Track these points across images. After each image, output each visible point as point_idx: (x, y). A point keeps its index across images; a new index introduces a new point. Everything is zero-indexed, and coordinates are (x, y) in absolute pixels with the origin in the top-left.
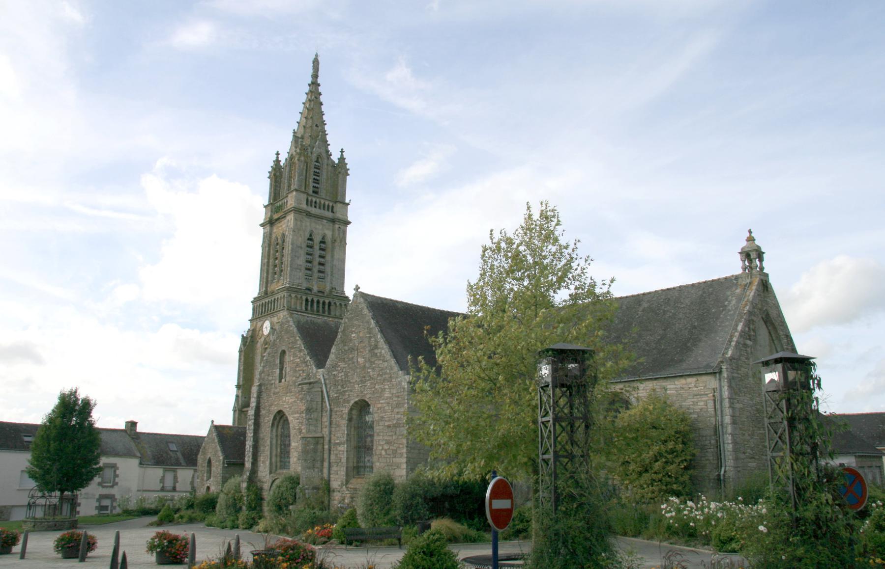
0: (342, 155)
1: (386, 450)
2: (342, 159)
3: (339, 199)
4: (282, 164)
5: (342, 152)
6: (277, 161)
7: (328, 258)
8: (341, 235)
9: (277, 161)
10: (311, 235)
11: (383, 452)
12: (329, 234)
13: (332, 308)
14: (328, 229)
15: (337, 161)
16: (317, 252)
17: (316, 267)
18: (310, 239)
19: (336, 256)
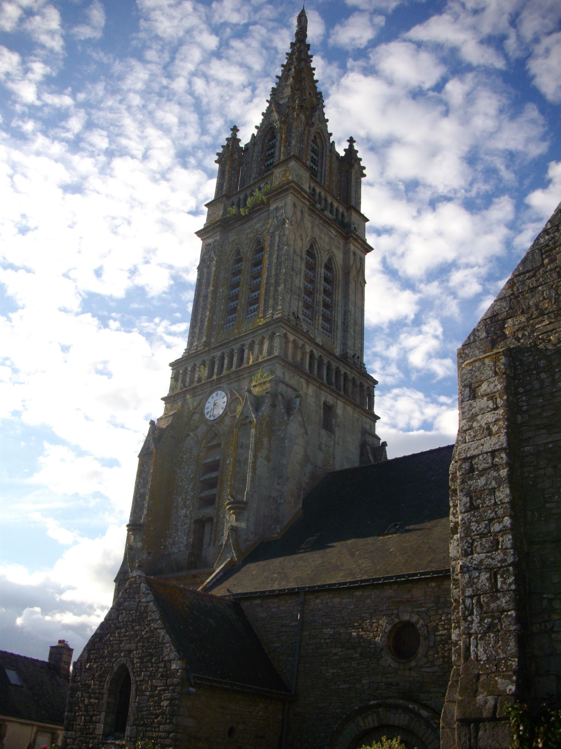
0: (351, 146)
2: (351, 152)
3: (353, 203)
4: (242, 145)
5: (351, 141)
6: (234, 140)
7: (339, 296)
8: (358, 263)
9: (234, 140)
10: (311, 247)
12: (339, 256)
13: (350, 384)
14: (338, 248)
15: (342, 154)
16: (321, 285)
17: (320, 297)
18: (310, 253)
19: (352, 298)
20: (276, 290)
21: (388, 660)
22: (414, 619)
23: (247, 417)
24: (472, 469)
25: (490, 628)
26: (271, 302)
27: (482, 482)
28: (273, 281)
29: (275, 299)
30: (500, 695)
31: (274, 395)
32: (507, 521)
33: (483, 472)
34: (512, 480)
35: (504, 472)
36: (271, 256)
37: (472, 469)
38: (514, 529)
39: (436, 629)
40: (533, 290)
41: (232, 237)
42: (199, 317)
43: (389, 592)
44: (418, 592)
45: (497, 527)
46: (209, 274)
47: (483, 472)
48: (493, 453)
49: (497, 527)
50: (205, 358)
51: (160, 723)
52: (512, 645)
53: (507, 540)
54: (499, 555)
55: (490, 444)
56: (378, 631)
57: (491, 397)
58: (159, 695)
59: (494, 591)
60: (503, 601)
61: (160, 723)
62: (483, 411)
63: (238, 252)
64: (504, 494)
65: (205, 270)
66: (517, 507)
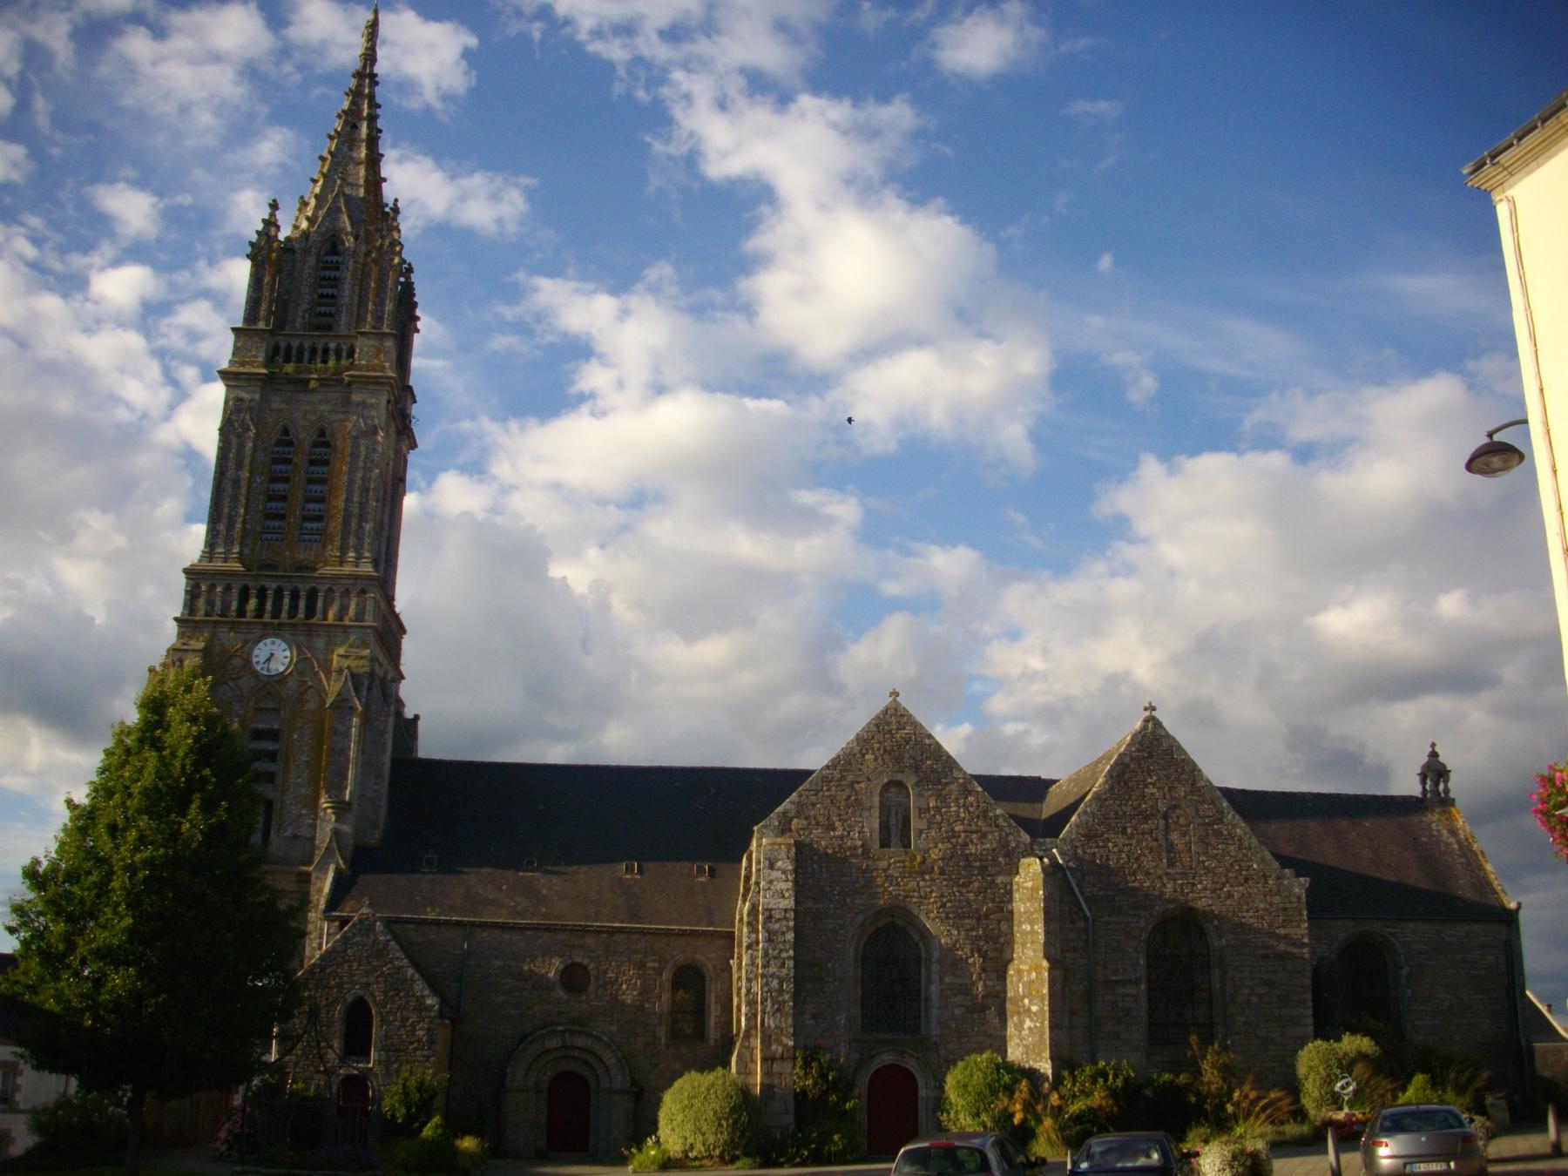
1: (1260, 996)
11: (1254, 999)
20: (360, 527)
21: (561, 993)
22: (586, 962)
23: (346, 700)
24: (770, 917)
25: (778, 1010)
26: (352, 541)
27: (777, 926)
28: (356, 510)
29: (360, 539)
30: (785, 1046)
31: (372, 675)
32: (791, 952)
33: (778, 920)
34: (796, 929)
35: (791, 924)
36: (352, 471)
37: (770, 917)
38: (795, 958)
39: (606, 972)
40: (814, 805)
41: (277, 402)
42: (226, 510)
43: (562, 936)
44: (590, 941)
45: (784, 955)
46: (241, 447)
47: (778, 920)
48: (786, 911)
49: (784, 955)
50: (251, 584)
51: (415, 1050)
52: (790, 1021)
53: (791, 964)
54: (785, 971)
55: (784, 904)
56: (552, 969)
57: (784, 872)
58: (413, 1025)
59: (781, 991)
60: (787, 997)
61: (415, 1050)
62: (778, 879)
63: (286, 432)
64: (790, 936)
65: (234, 441)
66: (799, 944)
